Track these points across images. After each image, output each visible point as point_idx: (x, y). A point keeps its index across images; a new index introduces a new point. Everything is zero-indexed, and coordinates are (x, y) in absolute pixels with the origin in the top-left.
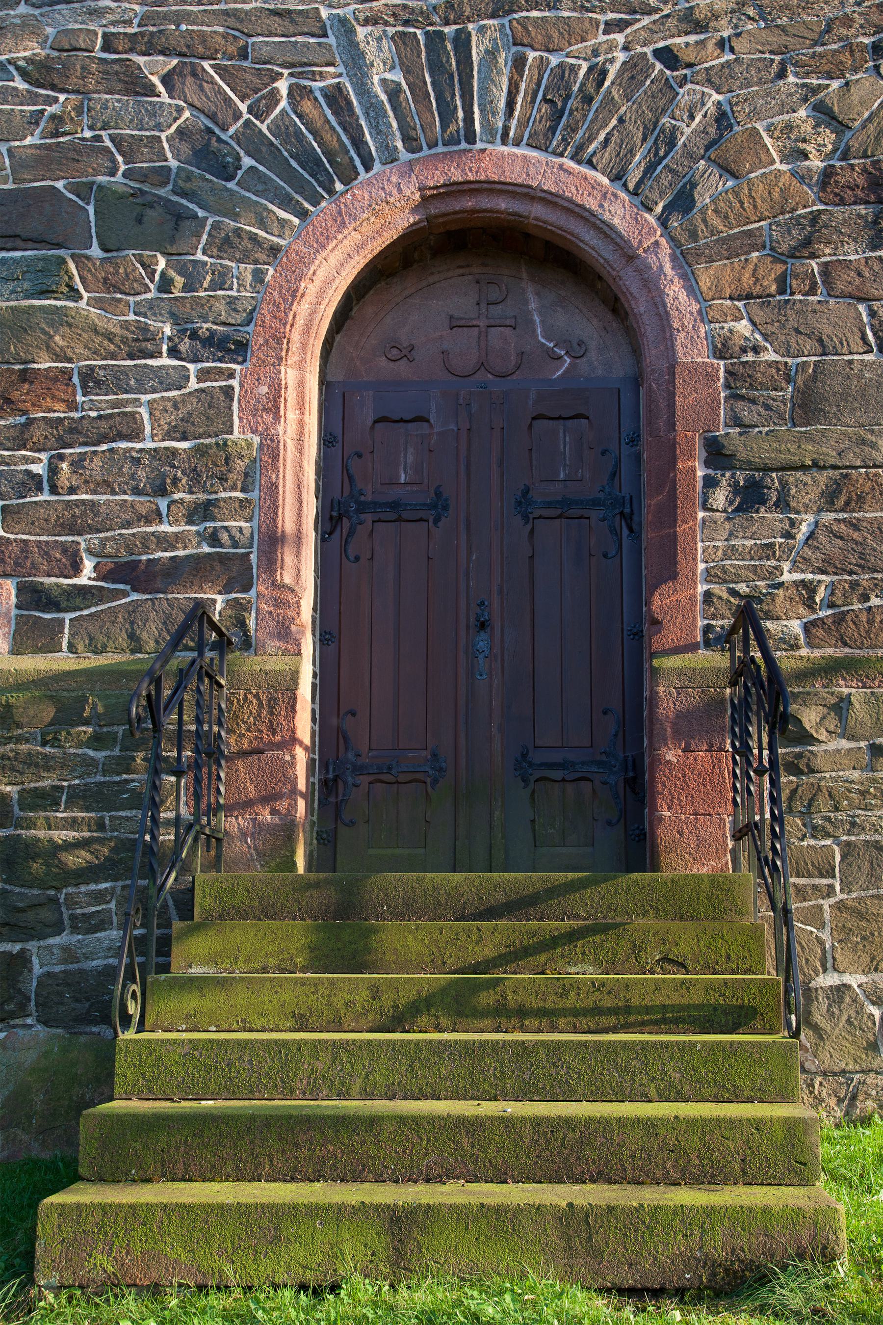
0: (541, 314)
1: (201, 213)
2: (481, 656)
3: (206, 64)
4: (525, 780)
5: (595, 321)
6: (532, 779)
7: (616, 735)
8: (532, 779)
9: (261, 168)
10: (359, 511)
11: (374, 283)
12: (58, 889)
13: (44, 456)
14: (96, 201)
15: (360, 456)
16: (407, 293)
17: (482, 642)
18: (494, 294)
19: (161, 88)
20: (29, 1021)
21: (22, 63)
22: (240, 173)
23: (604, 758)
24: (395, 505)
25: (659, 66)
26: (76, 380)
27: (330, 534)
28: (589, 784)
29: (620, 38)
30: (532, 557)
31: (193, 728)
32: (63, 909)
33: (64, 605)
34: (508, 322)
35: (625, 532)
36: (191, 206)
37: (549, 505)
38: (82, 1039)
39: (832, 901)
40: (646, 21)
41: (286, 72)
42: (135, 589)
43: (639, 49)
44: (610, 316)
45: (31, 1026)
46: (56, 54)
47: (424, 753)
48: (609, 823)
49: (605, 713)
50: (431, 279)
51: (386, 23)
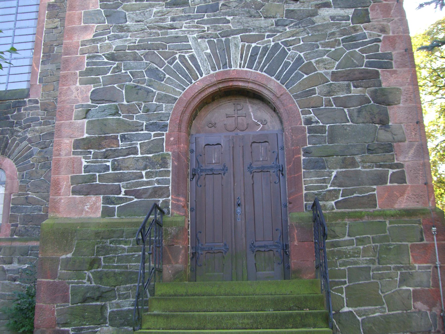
0: (253, 113)
1: (154, 91)
2: (239, 214)
3: (156, 51)
4: (253, 252)
5: (269, 114)
6: (255, 251)
7: (280, 237)
8: (255, 251)
9: (171, 77)
10: (201, 172)
11: (204, 106)
12: (115, 286)
13: (111, 160)
14: (125, 89)
15: (201, 156)
16: (214, 108)
17: (239, 210)
18: (239, 107)
19: (144, 58)
20: (107, 325)
21: (106, 55)
22: (165, 79)
23: (277, 244)
24: (211, 170)
25: (283, 46)
26: (119, 138)
27: (192, 179)
28: (272, 252)
29: (271, 39)
30: (253, 184)
31: (154, 238)
32: (116, 292)
33: (116, 203)
34: (243, 115)
35: (281, 175)
36: (152, 89)
37: (258, 168)
38: (122, 330)
39: (345, 286)
40: (278, 34)
41: (178, 52)
42: (135, 198)
43: (277, 42)
44: (273, 112)
45: (108, 326)
46: (115, 52)
47: (222, 244)
48: (279, 264)
49: (277, 230)
50: (220, 104)
51: (205, 38)
